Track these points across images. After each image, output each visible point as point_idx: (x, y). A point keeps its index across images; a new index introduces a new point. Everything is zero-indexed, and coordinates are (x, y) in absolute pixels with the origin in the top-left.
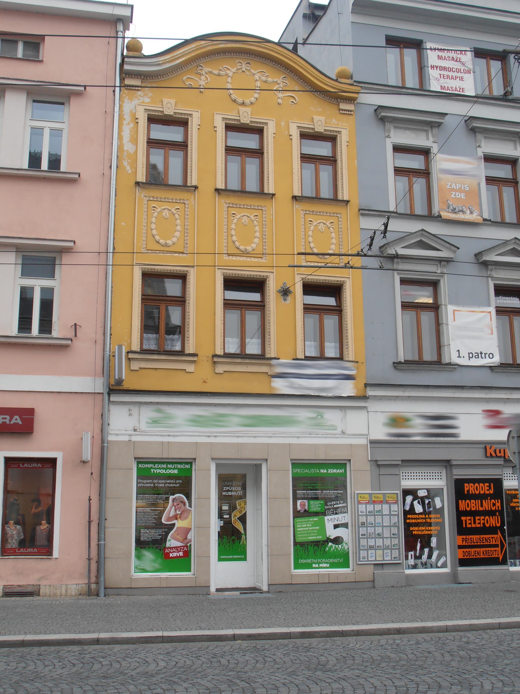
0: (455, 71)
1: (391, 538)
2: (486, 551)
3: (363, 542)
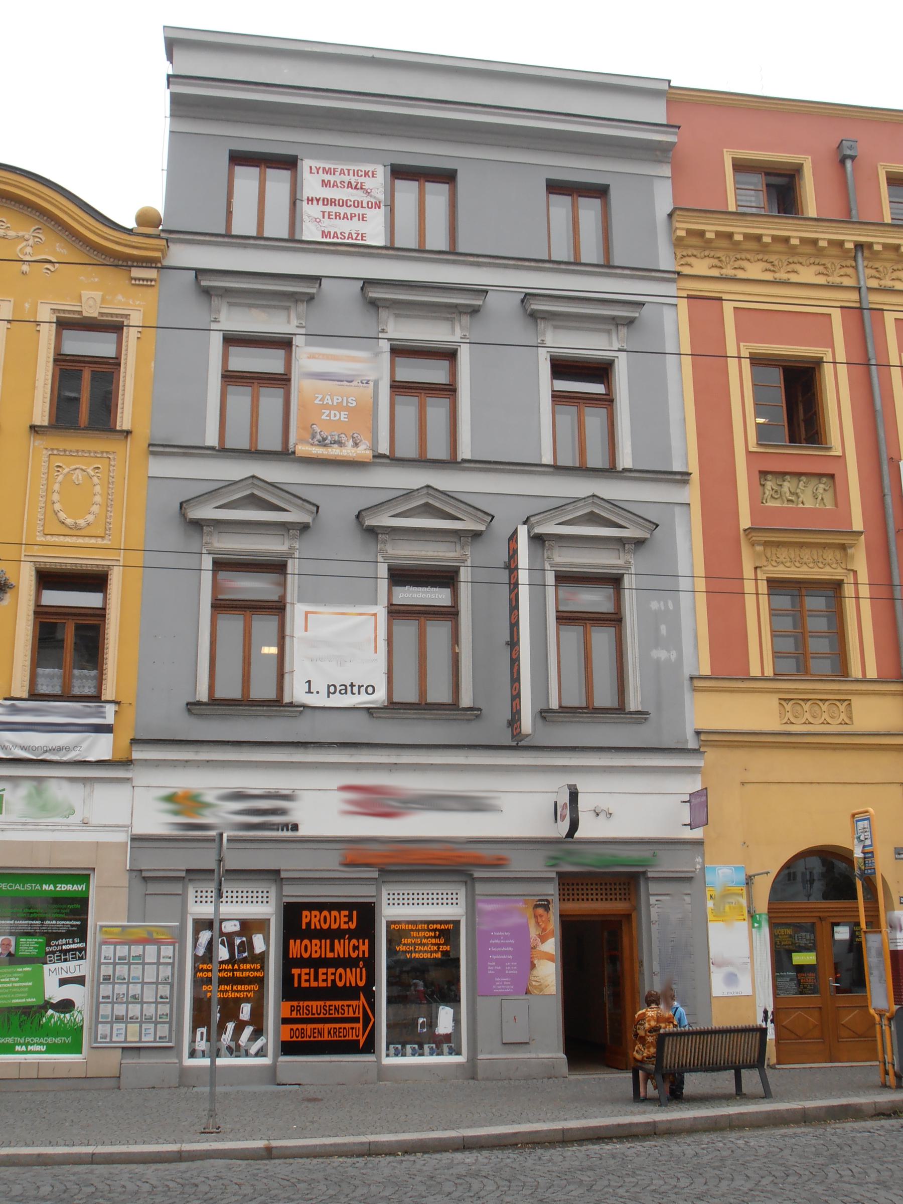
0: (351, 206)
1: (156, 1003)
2: (334, 1028)
3: (105, 1010)
